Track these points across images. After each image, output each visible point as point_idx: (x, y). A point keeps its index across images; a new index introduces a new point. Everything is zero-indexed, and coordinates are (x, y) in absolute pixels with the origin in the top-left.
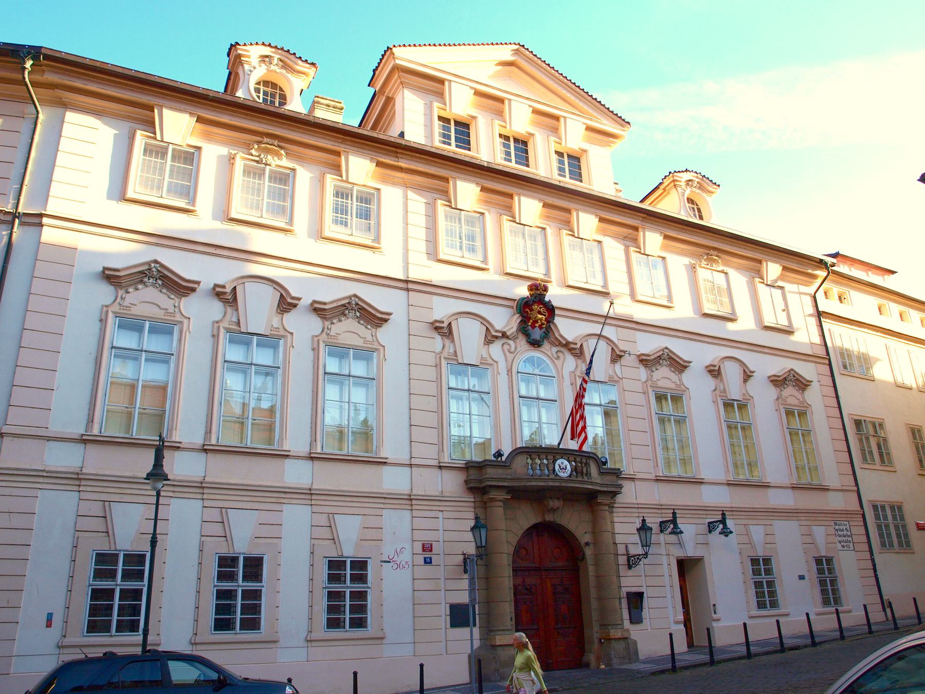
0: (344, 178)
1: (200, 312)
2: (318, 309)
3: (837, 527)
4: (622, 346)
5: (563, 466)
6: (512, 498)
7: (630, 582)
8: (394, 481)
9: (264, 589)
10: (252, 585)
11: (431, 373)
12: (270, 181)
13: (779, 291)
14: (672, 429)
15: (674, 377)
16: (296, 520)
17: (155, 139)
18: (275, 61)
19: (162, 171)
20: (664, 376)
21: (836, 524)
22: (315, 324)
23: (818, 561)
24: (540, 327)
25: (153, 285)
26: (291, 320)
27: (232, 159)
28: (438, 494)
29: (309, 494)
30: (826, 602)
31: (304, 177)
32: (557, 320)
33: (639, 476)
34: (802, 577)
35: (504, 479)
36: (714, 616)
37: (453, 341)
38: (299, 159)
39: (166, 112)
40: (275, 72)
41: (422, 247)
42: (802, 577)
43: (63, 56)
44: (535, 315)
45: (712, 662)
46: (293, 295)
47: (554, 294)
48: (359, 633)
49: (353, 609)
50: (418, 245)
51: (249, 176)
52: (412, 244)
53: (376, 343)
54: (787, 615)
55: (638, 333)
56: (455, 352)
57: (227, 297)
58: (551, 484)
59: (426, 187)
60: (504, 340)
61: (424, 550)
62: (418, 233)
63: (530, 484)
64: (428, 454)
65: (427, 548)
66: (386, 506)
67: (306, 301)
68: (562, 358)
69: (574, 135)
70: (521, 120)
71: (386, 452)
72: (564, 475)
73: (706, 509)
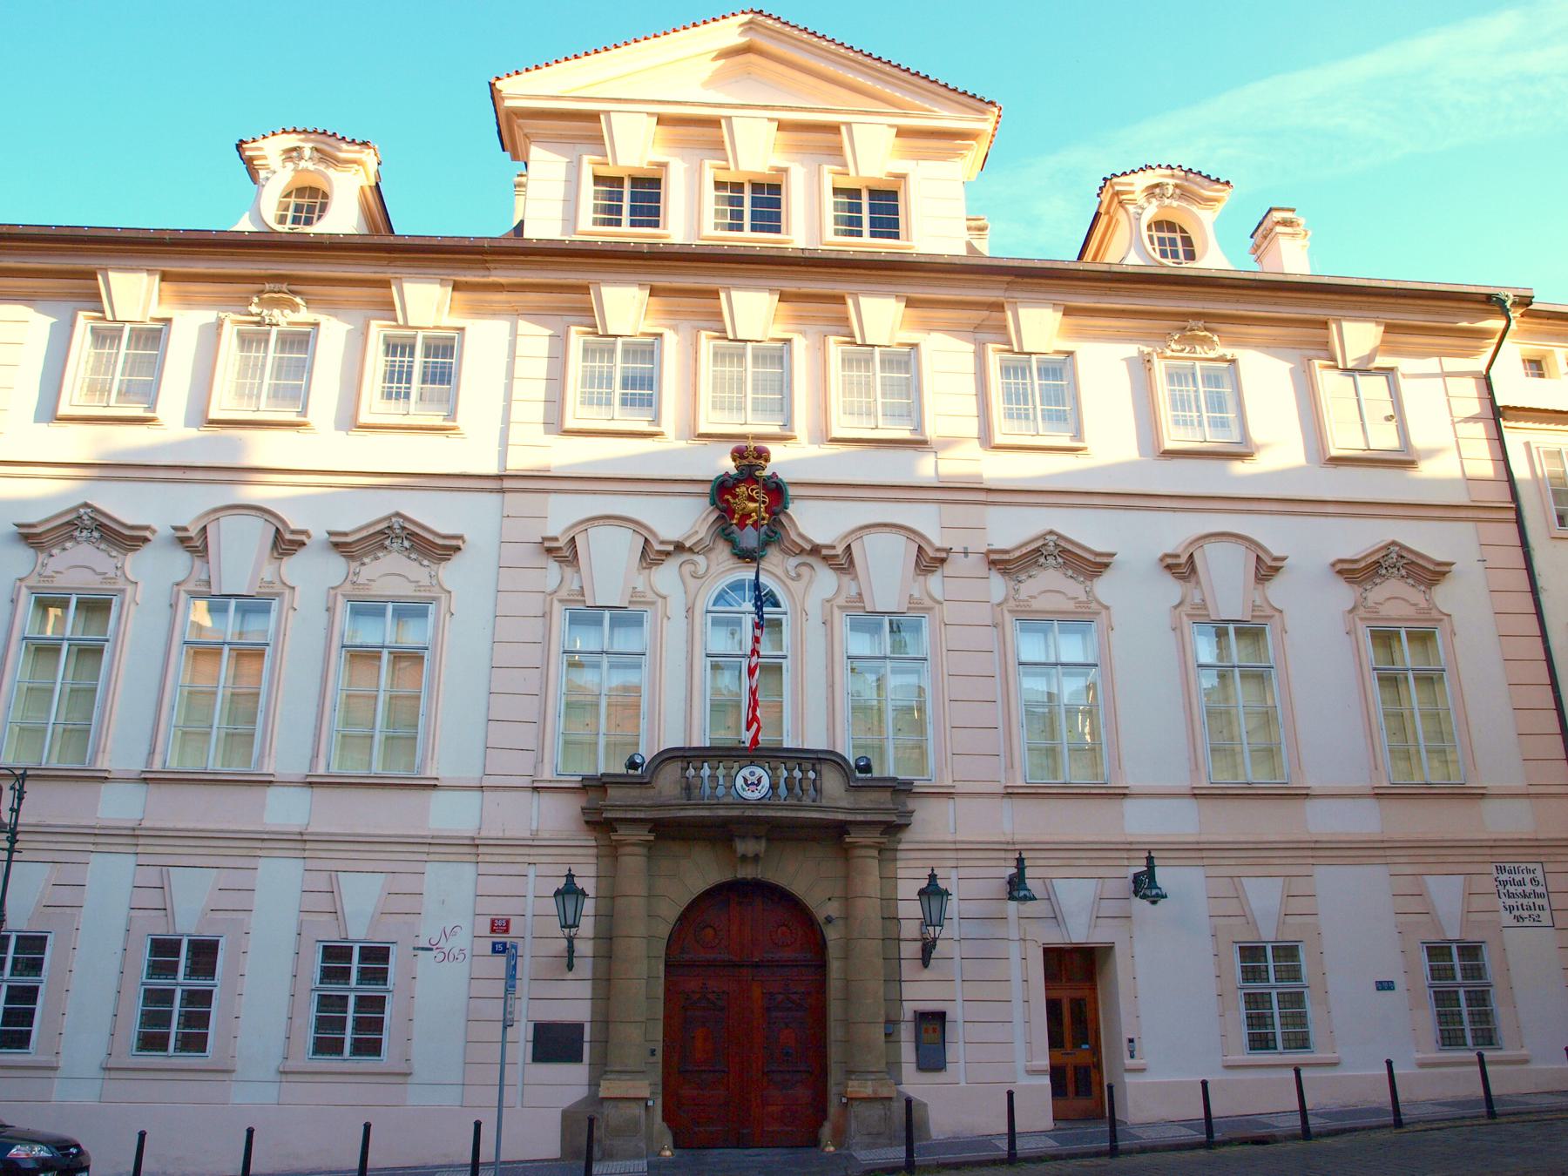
0: (401, 322)
1: (150, 575)
2: (341, 546)
3: (1504, 877)
4: (937, 538)
5: (751, 779)
6: (657, 838)
7: (920, 992)
8: (451, 815)
9: (216, 990)
10: (199, 984)
11: (535, 629)
12: (883, 369)
13: (1381, 381)
14: (1414, 695)
15: (1415, 595)
16: (279, 884)
17: (104, 319)
18: (307, 153)
19: (868, 387)
20: (1395, 599)
21: (1500, 870)
22: (335, 568)
23: (1437, 952)
24: (755, 524)
25: (88, 540)
26: (294, 568)
27: (220, 324)
28: (527, 835)
29: (300, 841)
30: (1450, 1038)
31: (333, 332)
32: (794, 509)
33: (960, 787)
34: (1385, 986)
35: (633, 807)
36: (1128, 1062)
37: (855, 578)
38: (330, 305)
39: (112, 275)
40: (306, 170)
41: (538, 412)
42: (1385, 986)
43: (53, 231)
44: (748, 503)
45: (1114, 1152)
46: (292, 527)
47: (782, 460)
48: (366, 1063)
49: (360, 1024)
50: (530, 410)
51: (851, 368)
52: (517, 411)
53: (437, 588)
54: (1143, 1070)
55: (990, 509)
56: (860, 594)
57: (194, 544)
58: (722, 813)
59: (558, 309)
60: (686, 556)
61: (493, 931)
62: (531, 390)
63: (683, 814)
64: (518, 768)
65: (500, 926)
66: (432, 857)
67: (319, 533)
68: (806, 578)
69: (874, 153)
70: (756, 150)
71: (439, 767)
72: (752, 795)
73: (1129, 848)
